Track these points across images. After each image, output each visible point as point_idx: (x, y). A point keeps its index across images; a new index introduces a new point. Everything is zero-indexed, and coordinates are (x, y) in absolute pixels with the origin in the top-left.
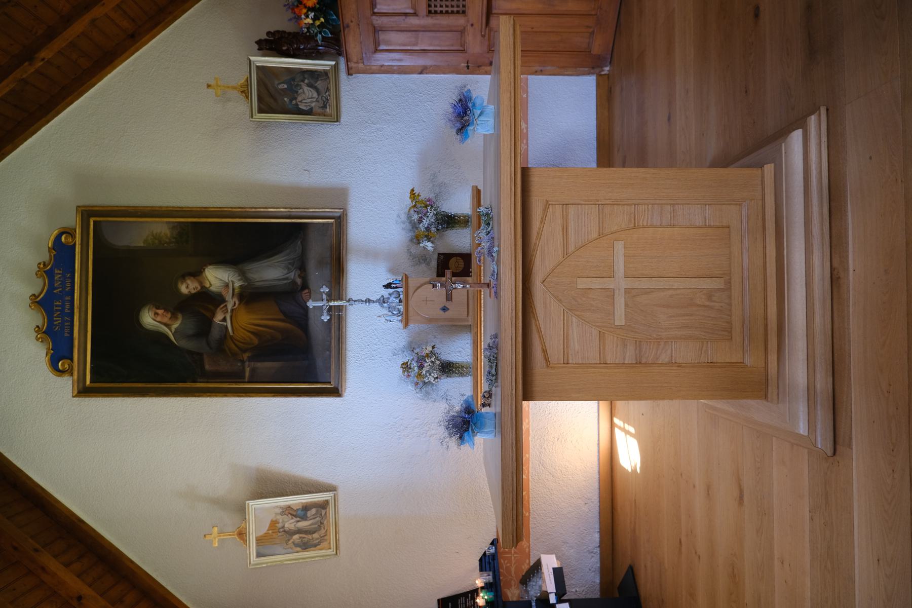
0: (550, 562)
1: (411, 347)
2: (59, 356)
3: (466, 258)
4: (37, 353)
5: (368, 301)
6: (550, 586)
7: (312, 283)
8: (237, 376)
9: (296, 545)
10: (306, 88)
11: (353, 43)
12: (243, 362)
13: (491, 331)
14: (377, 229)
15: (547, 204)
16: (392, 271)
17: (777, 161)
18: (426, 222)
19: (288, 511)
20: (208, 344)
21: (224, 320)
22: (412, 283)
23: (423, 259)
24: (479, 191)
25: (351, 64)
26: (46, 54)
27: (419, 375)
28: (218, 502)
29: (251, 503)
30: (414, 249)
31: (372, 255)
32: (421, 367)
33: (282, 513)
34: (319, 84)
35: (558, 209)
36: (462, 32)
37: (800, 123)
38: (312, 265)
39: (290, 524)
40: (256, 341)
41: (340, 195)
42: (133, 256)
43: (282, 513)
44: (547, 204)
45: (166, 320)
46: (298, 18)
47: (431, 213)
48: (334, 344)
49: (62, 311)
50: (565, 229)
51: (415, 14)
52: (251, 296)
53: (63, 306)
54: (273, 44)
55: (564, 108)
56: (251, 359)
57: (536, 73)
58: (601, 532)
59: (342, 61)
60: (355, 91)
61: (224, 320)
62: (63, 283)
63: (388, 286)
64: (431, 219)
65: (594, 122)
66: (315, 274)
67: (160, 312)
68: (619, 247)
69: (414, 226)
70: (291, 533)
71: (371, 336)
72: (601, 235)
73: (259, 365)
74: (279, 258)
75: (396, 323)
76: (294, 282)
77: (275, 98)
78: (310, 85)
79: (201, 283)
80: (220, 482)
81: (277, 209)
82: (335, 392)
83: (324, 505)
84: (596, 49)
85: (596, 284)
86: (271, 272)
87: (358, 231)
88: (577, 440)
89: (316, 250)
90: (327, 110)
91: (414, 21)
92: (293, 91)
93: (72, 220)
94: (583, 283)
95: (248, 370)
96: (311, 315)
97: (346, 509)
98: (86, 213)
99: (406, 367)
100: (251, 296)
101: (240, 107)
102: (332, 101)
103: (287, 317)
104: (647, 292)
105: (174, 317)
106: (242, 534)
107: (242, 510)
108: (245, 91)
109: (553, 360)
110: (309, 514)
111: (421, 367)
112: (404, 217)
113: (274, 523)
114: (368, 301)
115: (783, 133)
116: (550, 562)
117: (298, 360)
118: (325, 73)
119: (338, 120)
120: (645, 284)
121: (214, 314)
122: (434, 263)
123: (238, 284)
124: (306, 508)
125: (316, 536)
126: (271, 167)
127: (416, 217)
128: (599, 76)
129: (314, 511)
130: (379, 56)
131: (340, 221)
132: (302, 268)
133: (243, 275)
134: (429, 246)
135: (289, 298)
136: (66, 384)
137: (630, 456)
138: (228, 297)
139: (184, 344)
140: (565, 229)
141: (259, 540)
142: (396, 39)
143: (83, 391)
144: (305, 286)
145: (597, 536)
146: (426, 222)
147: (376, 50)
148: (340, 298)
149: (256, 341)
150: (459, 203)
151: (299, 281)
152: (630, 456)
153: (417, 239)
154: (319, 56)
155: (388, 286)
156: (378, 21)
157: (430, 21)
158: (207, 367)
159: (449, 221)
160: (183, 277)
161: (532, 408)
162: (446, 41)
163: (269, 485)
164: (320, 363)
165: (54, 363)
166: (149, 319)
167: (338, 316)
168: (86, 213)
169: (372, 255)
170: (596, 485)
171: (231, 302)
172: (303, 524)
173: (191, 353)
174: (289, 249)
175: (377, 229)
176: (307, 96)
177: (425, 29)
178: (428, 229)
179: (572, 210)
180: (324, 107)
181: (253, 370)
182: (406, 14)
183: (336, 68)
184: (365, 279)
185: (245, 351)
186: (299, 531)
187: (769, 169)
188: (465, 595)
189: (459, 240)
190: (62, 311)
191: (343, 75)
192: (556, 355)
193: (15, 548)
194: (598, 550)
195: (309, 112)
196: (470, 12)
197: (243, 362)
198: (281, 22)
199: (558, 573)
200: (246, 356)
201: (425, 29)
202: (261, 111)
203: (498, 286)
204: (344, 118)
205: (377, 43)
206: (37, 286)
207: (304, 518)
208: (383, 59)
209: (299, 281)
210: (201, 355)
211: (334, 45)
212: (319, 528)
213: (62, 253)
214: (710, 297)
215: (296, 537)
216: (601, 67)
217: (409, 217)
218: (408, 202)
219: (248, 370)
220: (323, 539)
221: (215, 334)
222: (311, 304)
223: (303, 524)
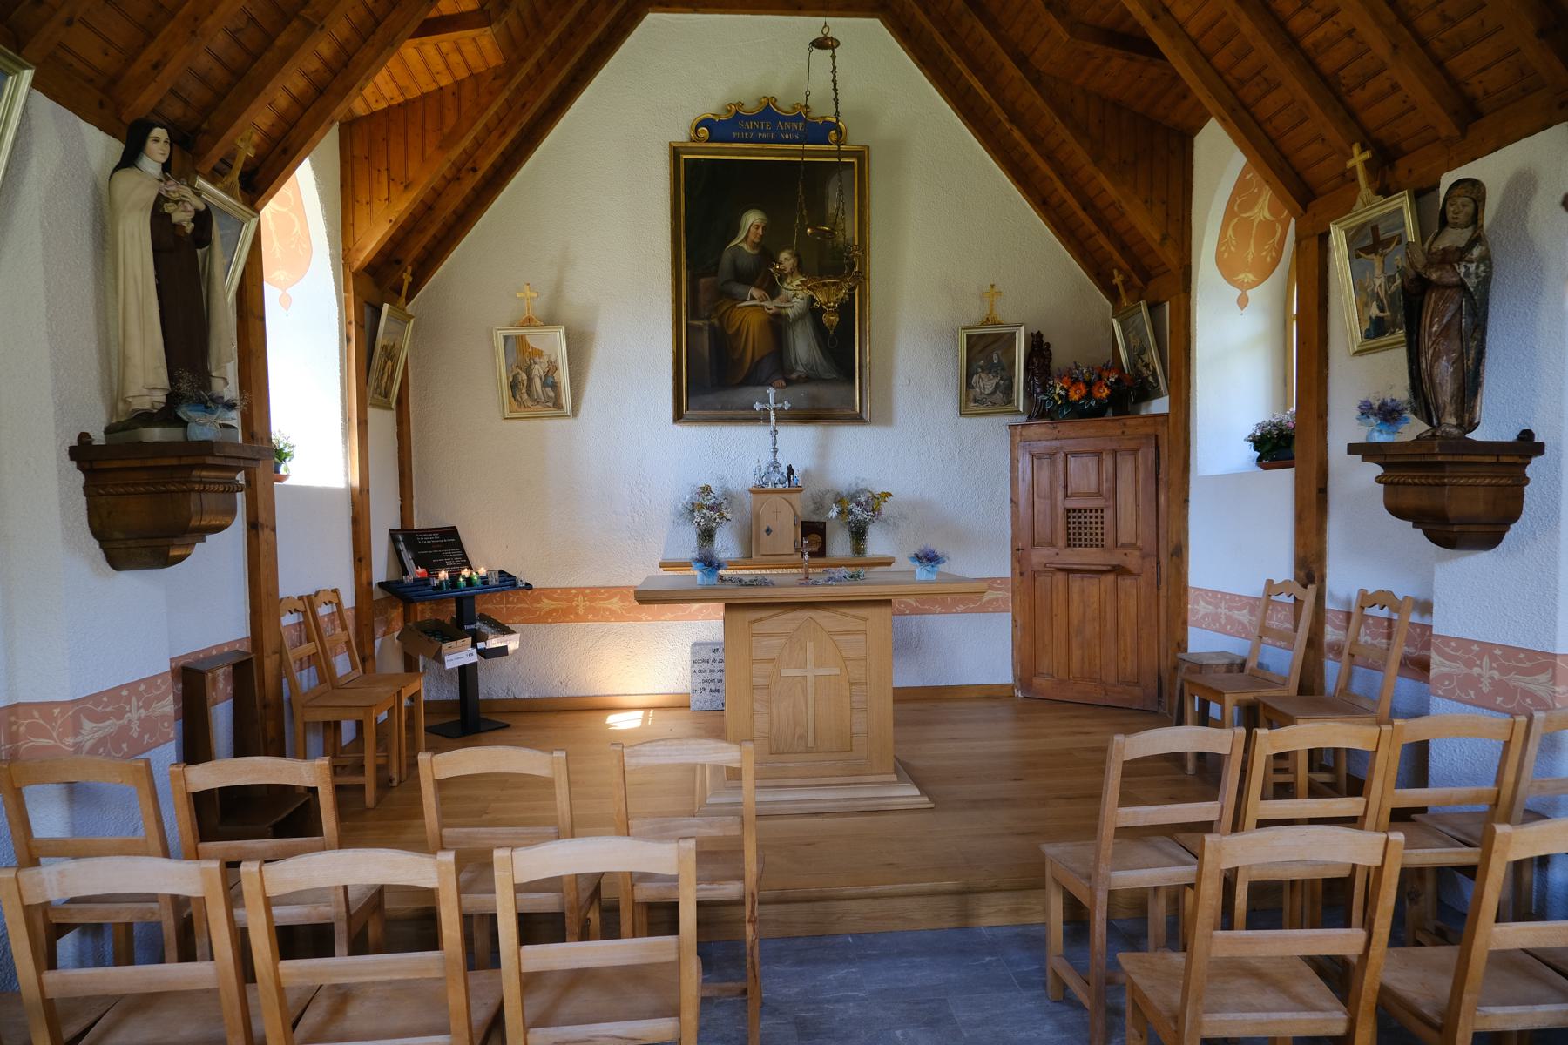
0: (512, 643)
1: (729, 496)
2: (716, 128)
3: (821, 552)
4: (711, 104)
5: (775, 451)
6: (494, 643)
7: (791, 390)
8: (693, 312)
9: (515, 377)
10: (994, 382)
11: (1038, 430)
12: (708, 318)
13: (775, 580)
14: (850, 457)
15: (866, 619)
16: (806, 473)
17: (900, 780)
18: (857, 510)
19: (552, 368)
20: (727, 282)
21: (753, 298)
22: (794, 497)
23: (819, 505)
24: (889, 564)
25: (1019, 429)
26: (1017, 134)
27: (702, 506)
28: (557, 291)
29: (563, 331)
30: (828, 499)
31: (823, 451)
32: (709, 508)
33: (550, 362)
34: (999, 395)
35: (862, 628)
36: (1051, 544)
37: (923, 793)
38: (812, 389)
39: (538, 370)
40: (731, 331)
41: (885, 418)
42: (817, 204)
43: (550, 362)
44: (866, 619)
45: (751, 237)
46: (1060, 378)
47: (866, 516)
48: (729, 413)
49: (760, 130)
50: (848, 633)
51: (1066, 496)
52: (778, 326)
53: (765, 131)
54: (1039, 349)
55: (980, 651)
56: (711, 326)
57: (1014, 620)
58: (531, 698)
59: (1022, 419)
60: (992, 432)
61: (753, 298)
62: (788, 131)
63: (791, 471)
64: (863, 512)
65: (964, 682)
66: (801, 392)
67: (760, 231)
68: (837, 671)
69: (853, 497)
70: (528, 371)
71: (737, 453)
72: (846, 659)
73: (706, 335)
74: (818, 356)
75: (752, 481)
76: (793, 370)
77: (983, 352)
78: (997, 386)
79: (791, 273)
80: (581, 293)
81: (868, 353)
82: (678, 416)
83: (557, 404)
84: (1037, 681)
85: (810, 656)
86: (803, 347)
87: (847, 437)
88: (641, 670)
89: (828, 394)
90: (971, 403)
91: (1060, 495)
92: (990, 369)
93: (854, 141)
94: (810, 645)
95: (700, 323)
96: (759, 389)
97: (553, 428)
98: (861, 155)
99: (706, 490)
100: (778, 326)
101: (973, 313)
102: (982, 409)
103: (756, 365)
104: (804, 691)
105: (755, 245)
106: (528, 322)
107: (550, 321)
108: (988, 322)
109: (755, 626)
110: (549, 390)
111: (709, 508)
112: (862, 485)
113: (540, 353)
114: (775, 451)
115: (918, 783)
116: (512, 643)
117: (714, 375)
118: (1010, 401)
119: (963, 412)
120: (810, 690)
121: (758, 287)
122: (815, 518)
123: (790, 311)
124: (555, 387)
125: (525, 396)
126: (913, 349)
127: (863, 499)
128: (1013, 687)
129: (552, 394)
130: (1028, 457)
131: (857, 419)
132: (808, 379)
133: (800, 317)
134: (833, 514)
135: (775, 365)
136: (681, 135)
137: (619, 722)
138: (777, 302)
139: (727, 256)
140: (848, 633)
141: (522, 337)
142: (1043, 476)
143: (676, 152)
144: (789, 383)
145: (527, 696)
146: (857, 510)
147: (1032, 456)
148: (778, 419)
149: (731, 331)
150: (877, 544)
151: (794, 376)
152: (619, 722)
153: (839, 500)
154: (1029, 394)
155: (791, 471)
156: (1060, 458)
157: (1060, 512)
158: (703, 280)
159: (859, 534)
160: (797, 256)
161: (719, 609)
162: (1043, 529)
163: (579, 346)
164: (710, 398)
165: (705, 122)
166: (752, 219)
167: (761, 418)
168: (861, 155)
169: (823, 451)
170: (581, 694)
171: (772, 306)
172: (538, 383)
173: (717, 264)
174: (830, 373)
175: (850, 457)
176: (986, 383)
177: (1052, 507)
178: (851, 512)
179: (862, 637)
180: (975, 401)
181: (700, 329)
182: (1066, 487)
183: (1017, 412)
184: (798, 445)
185: (721, 321)
186: (530, 379)
187: (894, 778)
188: (464, 556)
189: (839, 545)
190: (760, 130)
191: (1010, 420)
192: (757, 628)
193: (524, 105)
194: (511, 696)
195: (969, 386)
196: (1069, 551)
197: (708, 318)
198: (1061, 357)
199: (503, 651)
200: (715, 321)
201: (1052, 507)
202: (969, 337)
203: (807, 585)
204: (963, 419)
205: (1039, 456)
206: (785, 106)
207: (544, 384)
208: (1024, 462)
209: (794, 376)
210: (715, 274)
211: (1040, 412)
212: (533, 400)
213: (819, 131)
214: (801, 737)
215: (524, 376)
216: (1022, 688)
217: (863, 491)
218: (878, 490)
219: (700, 323)
220: (521, 404)
221: (738, 289)
222: (771, 391)
223: (538, 383)
